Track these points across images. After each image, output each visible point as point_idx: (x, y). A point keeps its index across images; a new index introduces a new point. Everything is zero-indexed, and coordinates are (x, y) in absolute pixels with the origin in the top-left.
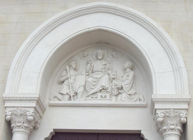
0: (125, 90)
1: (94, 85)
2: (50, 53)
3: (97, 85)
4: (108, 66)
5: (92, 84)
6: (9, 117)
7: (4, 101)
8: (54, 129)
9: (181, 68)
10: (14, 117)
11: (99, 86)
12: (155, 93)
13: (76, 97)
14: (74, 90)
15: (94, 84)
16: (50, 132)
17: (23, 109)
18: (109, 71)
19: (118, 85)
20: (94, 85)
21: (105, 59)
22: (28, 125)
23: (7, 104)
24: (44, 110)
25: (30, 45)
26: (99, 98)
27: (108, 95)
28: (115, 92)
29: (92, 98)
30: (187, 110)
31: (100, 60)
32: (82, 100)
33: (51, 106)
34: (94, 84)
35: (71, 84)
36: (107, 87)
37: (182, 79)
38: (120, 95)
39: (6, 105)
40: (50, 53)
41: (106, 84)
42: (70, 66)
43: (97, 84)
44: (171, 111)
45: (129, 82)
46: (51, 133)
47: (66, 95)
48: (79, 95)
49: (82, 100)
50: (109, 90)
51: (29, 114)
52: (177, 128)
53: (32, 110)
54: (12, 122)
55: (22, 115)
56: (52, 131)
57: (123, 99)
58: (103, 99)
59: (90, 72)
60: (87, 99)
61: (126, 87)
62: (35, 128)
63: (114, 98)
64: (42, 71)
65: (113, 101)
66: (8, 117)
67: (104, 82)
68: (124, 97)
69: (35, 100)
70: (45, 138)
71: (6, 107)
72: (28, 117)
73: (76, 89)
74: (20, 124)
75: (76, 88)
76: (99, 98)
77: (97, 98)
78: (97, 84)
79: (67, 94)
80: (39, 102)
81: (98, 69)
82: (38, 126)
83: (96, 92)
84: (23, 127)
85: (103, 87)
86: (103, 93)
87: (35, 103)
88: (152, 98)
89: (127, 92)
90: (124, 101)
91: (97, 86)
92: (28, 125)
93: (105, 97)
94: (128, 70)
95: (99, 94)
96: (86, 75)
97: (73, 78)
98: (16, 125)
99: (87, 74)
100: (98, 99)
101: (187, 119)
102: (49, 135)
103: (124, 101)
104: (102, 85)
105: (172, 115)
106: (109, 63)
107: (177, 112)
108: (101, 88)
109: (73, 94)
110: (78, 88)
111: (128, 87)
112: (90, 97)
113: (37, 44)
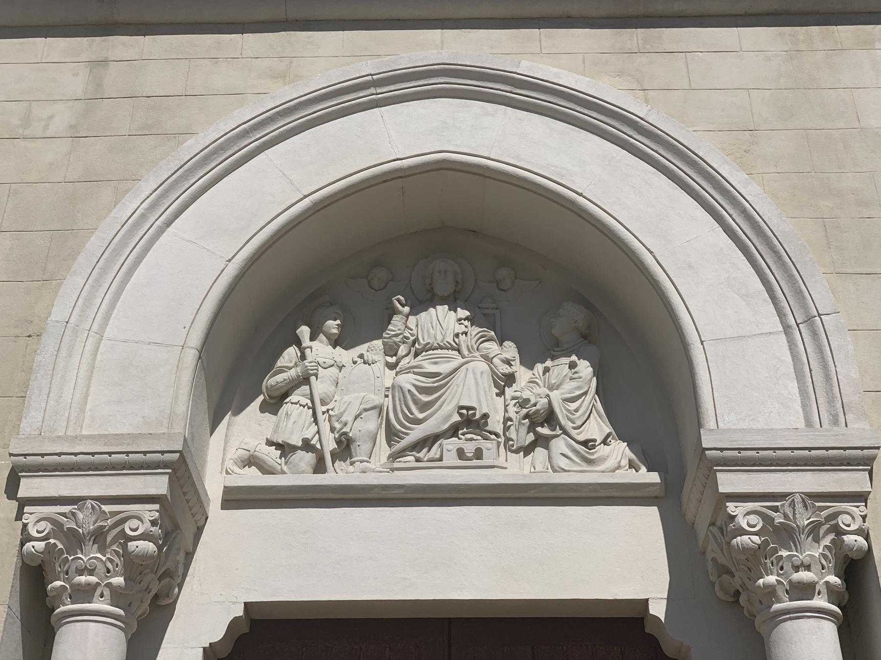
0: (563, 421)
2: (229, 261)
5: (416, 401)
6: (40, 545)
8: (245, 603)
12: (709, 422)
14: (338, 426)
15: (425, 398)
16: (234, 616)
18: (486, 345)
19: (533, 402)
23: (28, 487)
25: (137, 225)
29: (418, 460)
34: (425, 398)
36: (485, 411)
37: (831, 363)
40: (229, 261)
41: (479, 401)
43: (439, 398)
44: (793, 505)
45: (578, 388)
46: (234, 624)
47: (300, 453)
52: (827, 583)
53: (150, 512)
64: (196, 338)
70: (204, 649)
73: (346, 424)
75: (344, 419)
76: (451, 459)
77: (441, 459)
78: (439, 398)
84: (107, 592)
85: (464, 411)
87: (166, 478)
88: (704, 446)
89: (574, 433)
90: (565, 471)
91: (437, 411)
93: (479, 454)
95: (451, 444)
98: (72, 586)
99: (392, 360)
100: (445, 463)
101: (867, 538)
103: (565, 471)
105: (804, 519)
106: (484, 315)
108: (456, 418)
110: (356, 418)
112: (412, 458)
113: (169, 223)
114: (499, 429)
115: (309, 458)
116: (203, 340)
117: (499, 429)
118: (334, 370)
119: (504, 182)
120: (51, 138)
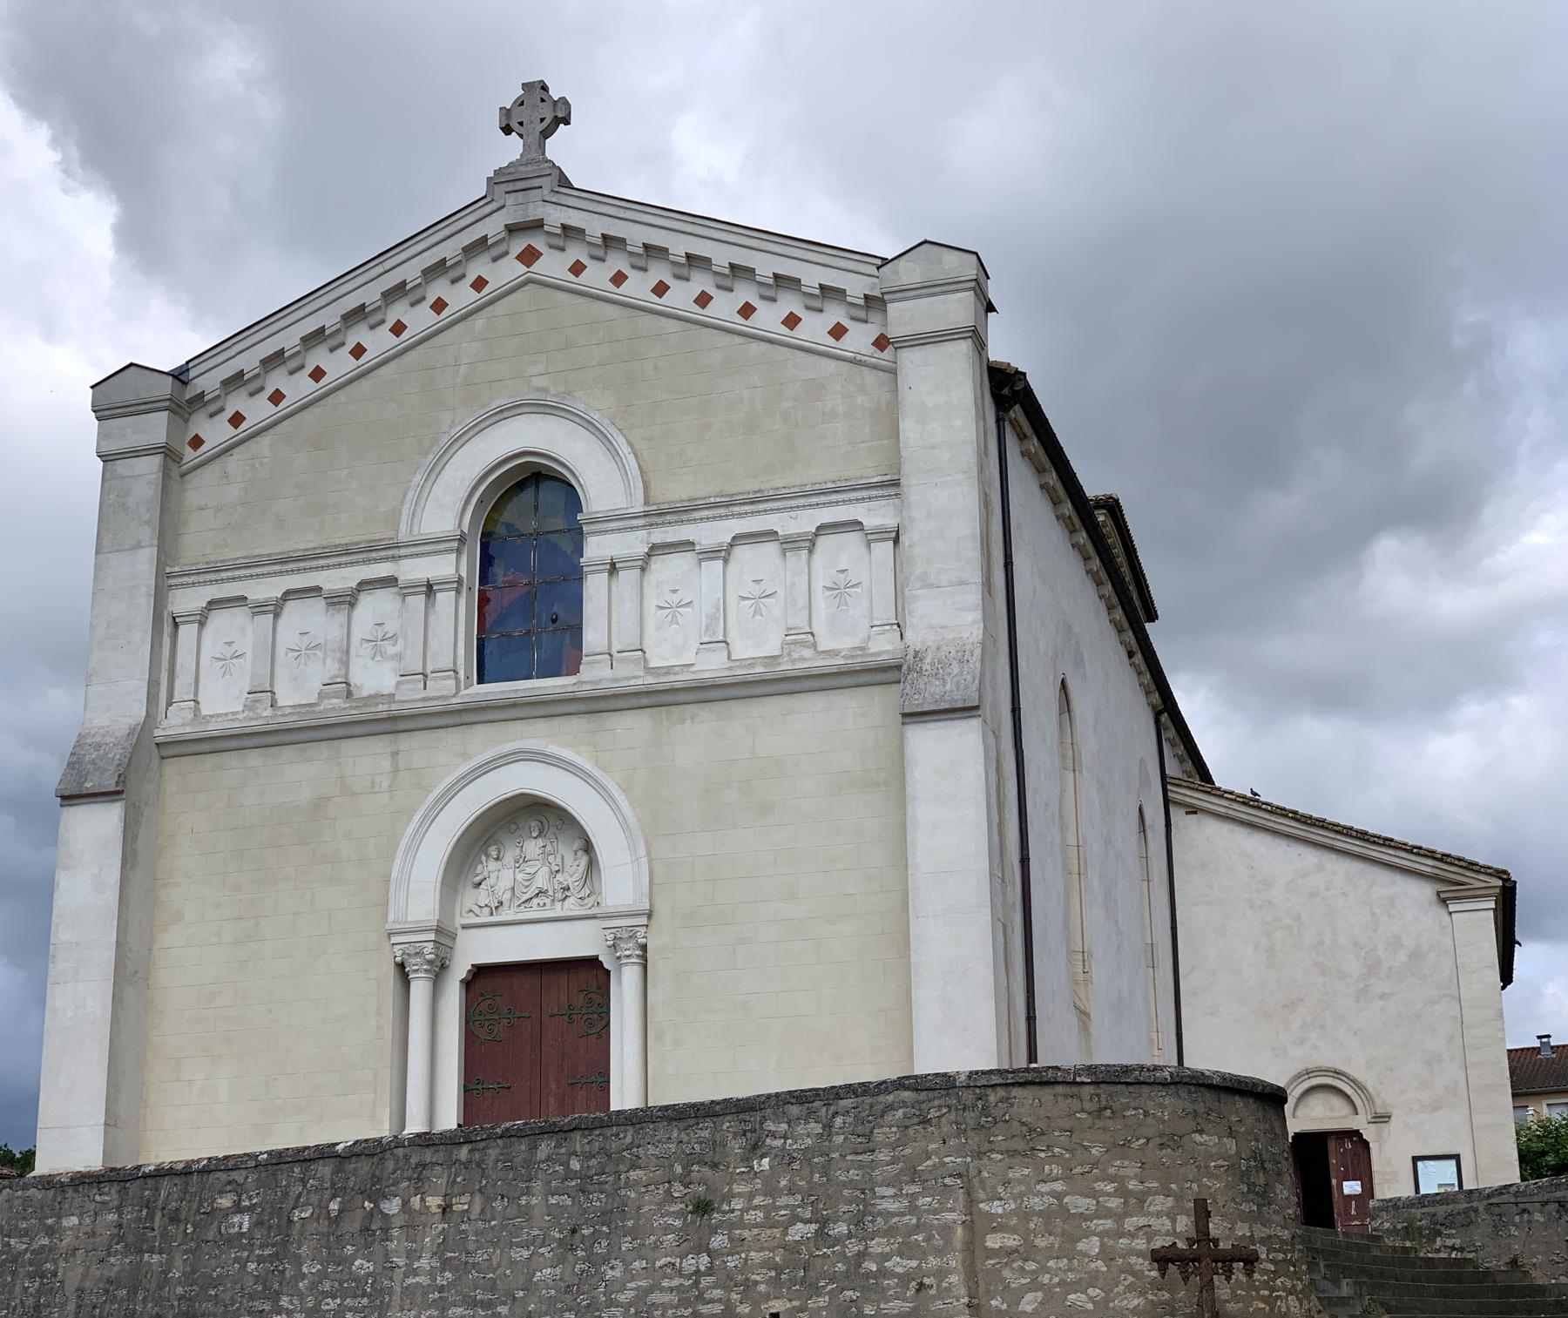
1: (527, 887)
4: (549, 848)
7: (390, 935)
11: (534, 887)
13: (500, 909)
17: (418, 945)
20: (527, 887)
21: (544, 833)
22: (429, 968)
23: (395, 939)
24: (453, 937)
27: (548, 901)
28: (559, 895)
30: (647, 926)
31: (535, 838)
33: (464, 927)
34: (527, 884)
35: (491, 887)
38: (567, 900)
39: (392, 942)
42: (488, 856)
48: (506, 904)
50: (550, 893)
53: (431, 945)
54: (406, 965)
55: (417, 954)
57: (571, 907)
58: (540, 908)
59: (521, 861)
62: (443, 967)
63: (558, 905)
65: (558, 911)
66: (399, 959)
67: (541, 881)
71: (393, 944)
72: (427, 957)
74: (416, 967)
76: (535, 908)
79: (486, 905)
80: (439, 930)
82: (448, 962)
83: (531, 899)
87: (434, 935)
89: (576, 895)
92: (429, 968)
93: (545, 904)
94: (580, 853)
95: (535, 901)
96: (515, 867)
97: (493, 876)
107: (631, 931)
108: (537, 892)
109: (497, 904)
113: (426, 831)
114: (552, 894)
115: (487, 910)
116: (430, 1042)
117: (552, 894)
118: (497, 873)
119: (420, 253)
120: (584, 210)
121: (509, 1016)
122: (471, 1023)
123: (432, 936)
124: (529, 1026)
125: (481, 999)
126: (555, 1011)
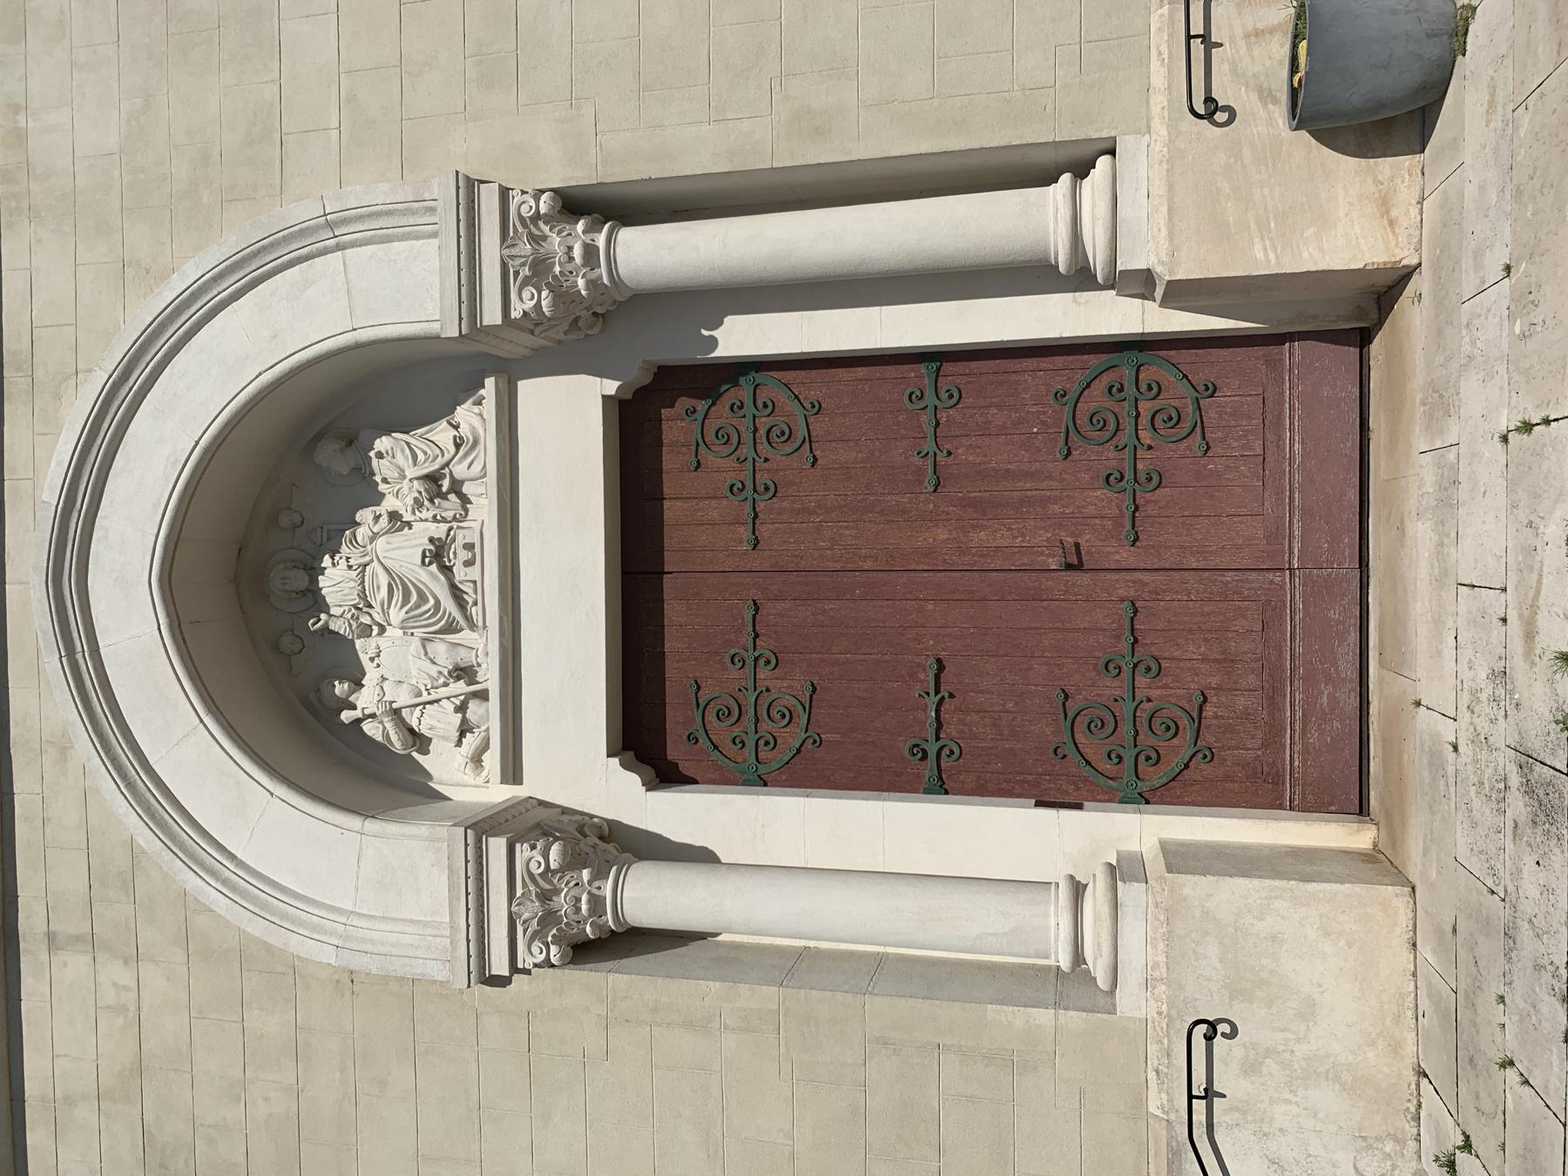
0: (436, 466)
2: (272, 794)
3: (419, 584)
5: (417, 606)
6: (554, 949)
8: (608, 756)
9: (325, 215)
10: (1557, 866)
12: (434, 328)
14: (442, 680)
18: (359, 539)
19: (417, 495)
20: (423, 598)
26: (473, 574)
29: (475, 604)
32: (486, 645)
40: (272, 794)
43: (397, 575)
46: (624, 765)
47: (469, 714)
49: (486, 645)
51: (540, 864)
53: (523, 852)
56: (615, 761)
60: (480, 624)
61: (425, 462)
64: (354, 822)
65: (484, 510)
68: (469, 467)
69: (480, 841)
70: (647, 790)
73: (440, 673)
75: (435, 675)
76: (473, 574)
81: (352, 584)
85: (427, 560)
86: (451, 556)
88: (457, 335)
89: (447, 456)
95: (460, 573)
98: (590, 916)
99: (376, 630)
101: (542, 192)
102: (639, 780)
104: (419, 563)
106: (328, 540)
108: (434, 567)
111: (425, 453)
112: (474, 609)
113: (232, 857)
118: (386, 685)
121: (750, 662)
122: (762, 770)
123: (497, 847)
124: (780, 606)
125: (703, 740)
126: (744, 532)
